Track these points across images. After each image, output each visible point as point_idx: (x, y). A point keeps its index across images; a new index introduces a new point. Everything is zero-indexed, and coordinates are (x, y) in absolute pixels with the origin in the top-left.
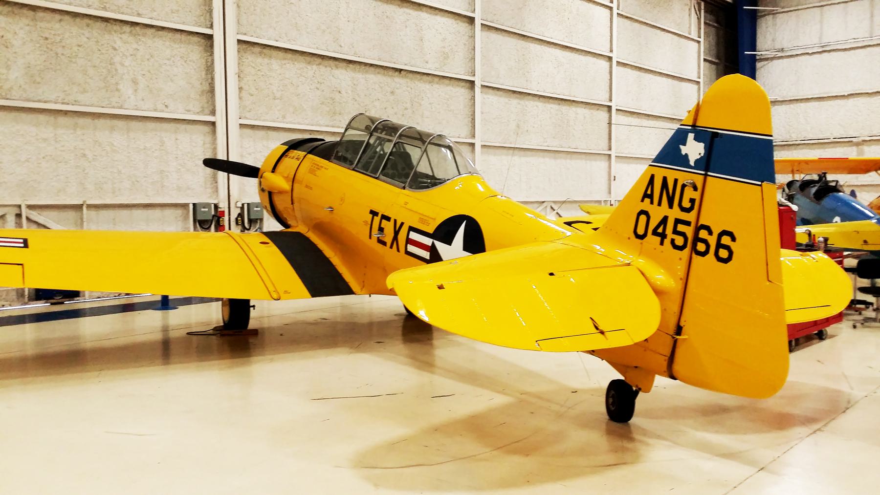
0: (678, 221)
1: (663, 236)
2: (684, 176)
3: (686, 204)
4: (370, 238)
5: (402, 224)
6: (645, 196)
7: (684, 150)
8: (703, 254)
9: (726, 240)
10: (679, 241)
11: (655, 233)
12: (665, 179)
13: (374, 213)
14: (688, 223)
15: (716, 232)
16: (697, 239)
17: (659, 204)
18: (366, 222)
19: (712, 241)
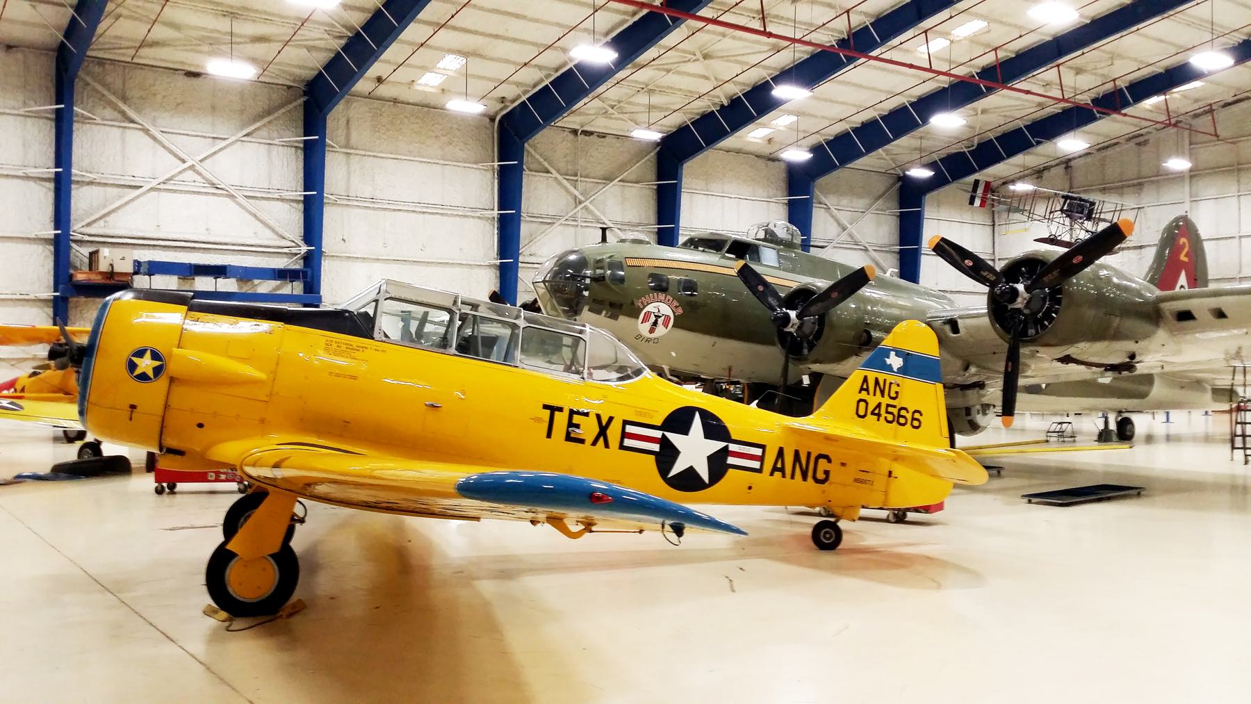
0: (888, 406)
1: (879, 415)
2: (890, 378)
3: (820, 476)
4: (549, 436)
5: (611, 419)
6: (862, 389)
7: (888, 361)
8: (903, 425)
9: (917, 416)
10: (890, 417)
11: (873, 413)
12: (877, 379)
13: (553, 409)
14: (894, 407)
15: (911, 411)
16: (900, 416)
17: (793, 477)
18: (538, 420)
19: (909, 416)
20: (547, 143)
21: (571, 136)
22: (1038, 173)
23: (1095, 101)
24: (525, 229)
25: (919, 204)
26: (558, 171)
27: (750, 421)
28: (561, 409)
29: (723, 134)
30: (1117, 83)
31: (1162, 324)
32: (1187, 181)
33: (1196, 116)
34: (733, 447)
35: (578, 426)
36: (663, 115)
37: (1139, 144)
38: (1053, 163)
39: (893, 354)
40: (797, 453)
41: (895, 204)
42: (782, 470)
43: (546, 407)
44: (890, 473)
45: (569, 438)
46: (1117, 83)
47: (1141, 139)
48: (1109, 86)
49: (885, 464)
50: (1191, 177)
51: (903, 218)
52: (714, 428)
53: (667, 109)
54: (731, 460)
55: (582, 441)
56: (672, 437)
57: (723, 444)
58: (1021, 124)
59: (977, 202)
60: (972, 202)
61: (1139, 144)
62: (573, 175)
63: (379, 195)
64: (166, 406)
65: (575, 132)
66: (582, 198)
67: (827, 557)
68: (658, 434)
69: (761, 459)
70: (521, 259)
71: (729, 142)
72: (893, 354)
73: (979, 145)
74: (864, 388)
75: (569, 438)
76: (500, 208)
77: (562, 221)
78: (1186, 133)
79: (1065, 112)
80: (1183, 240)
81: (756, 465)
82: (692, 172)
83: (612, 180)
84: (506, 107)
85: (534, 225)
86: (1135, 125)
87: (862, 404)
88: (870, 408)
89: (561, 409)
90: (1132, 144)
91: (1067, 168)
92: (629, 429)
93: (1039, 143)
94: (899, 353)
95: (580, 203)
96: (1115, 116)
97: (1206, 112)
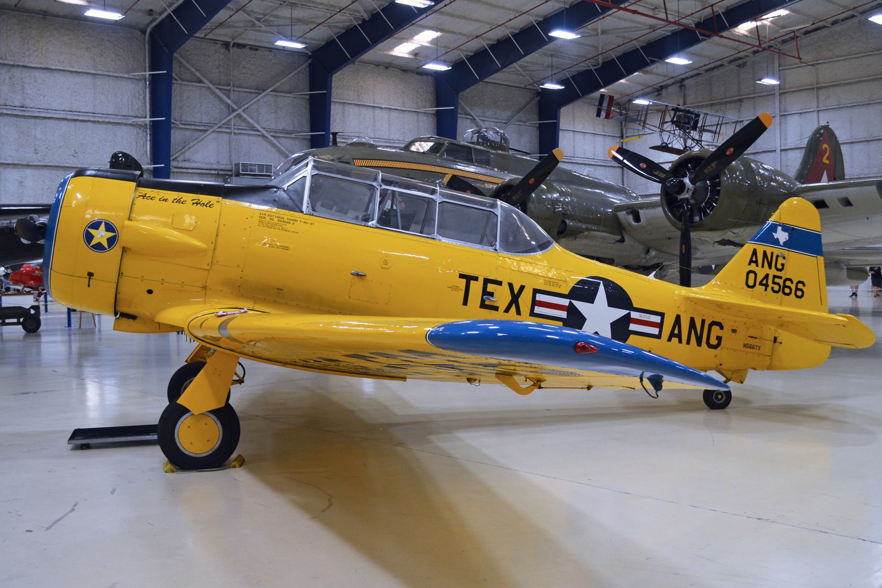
0: (775, 277)
1: (766, 286)
2: (777, 251)
5: (522, 288)
7: (776, 236)
9: (800, 286)
10: (776, 288)
11: (761, 284)
12: (765, 252)
13: (469, 279)
14: (780, 278)
15: (795, 282)
16: (785, 286)
17: (688, 343)
18: (455, 288)
19: (793, 287)
20: (193, 53)
21: (223, 50)
22: (658, 91)
23: (698, 25)
24: (176, 136)
25: (556, 116)
26: (211, 82)
27: (647, 289)
28: (476, 279)
29: (365, 47)
30: (715, 9)
31: (563, 240)
32: (777, 97)
33: (784, 42)
34: (634, 315)
35: (492, 294)
36: (307, 28)
37: (739, 66)
38: (670, 82)
39: (779, 228)
40: (692, 320)
41: (536, 117)
42: (679, 336)
43: (462, 276)
44: (775, 338)
45: (483, 305)
46: (715, 9)
47: (740, 62)
48: (708, 11)
49: (770, 331)
50: (781, 94)
51: (541, 127)
52: (618, 297)
53: (312, 23)
54: (633, 327)
55: (496, 309)
56: (580, 305)
57: (625, 312)
58: (637, 44)
59: (603, 114)
60: (598, 115)
61: (739, 66)
62: (227, 86)
63: (28, 103)
64: (120, 274)
65: (226, 45)
66: (236, 107)
67: (717, 416)
68: (565, 302)
69: (660, 326)
70: (173, 164)
71: (370, 55)
72: (779, 228)
73: (603, 63)
74: (753, 260)
75: (483, 305)
76: (152, 116)
77: (215, 128)
78: (776, 56)
79: (674, 34)
80: (825, 146)
81: (655, 331)
82: (343, 84)
83: (264, 90)
84: (155, 19)
85: (188, 133)
86: (735, 49)
87: (752, 276)
88: (759, 280)
89: (476, 279)
90: (733, 66)
91: (681, 87)
92: (540, 297)
93: (653, 62)
94: (785, 228)
95: (234, 111)
96: (716, 38)
97: (792, 39)
